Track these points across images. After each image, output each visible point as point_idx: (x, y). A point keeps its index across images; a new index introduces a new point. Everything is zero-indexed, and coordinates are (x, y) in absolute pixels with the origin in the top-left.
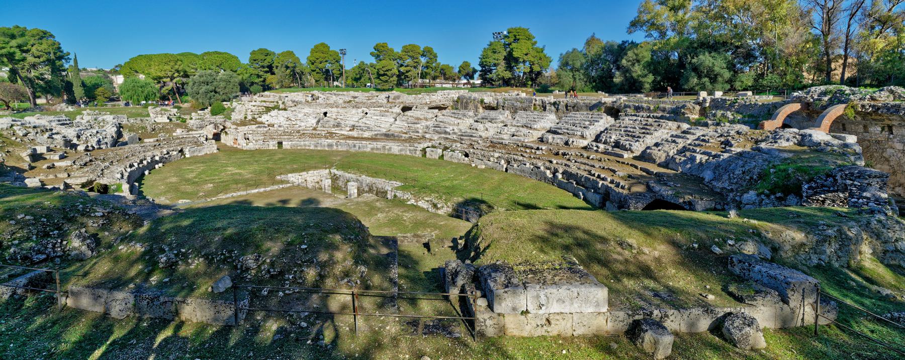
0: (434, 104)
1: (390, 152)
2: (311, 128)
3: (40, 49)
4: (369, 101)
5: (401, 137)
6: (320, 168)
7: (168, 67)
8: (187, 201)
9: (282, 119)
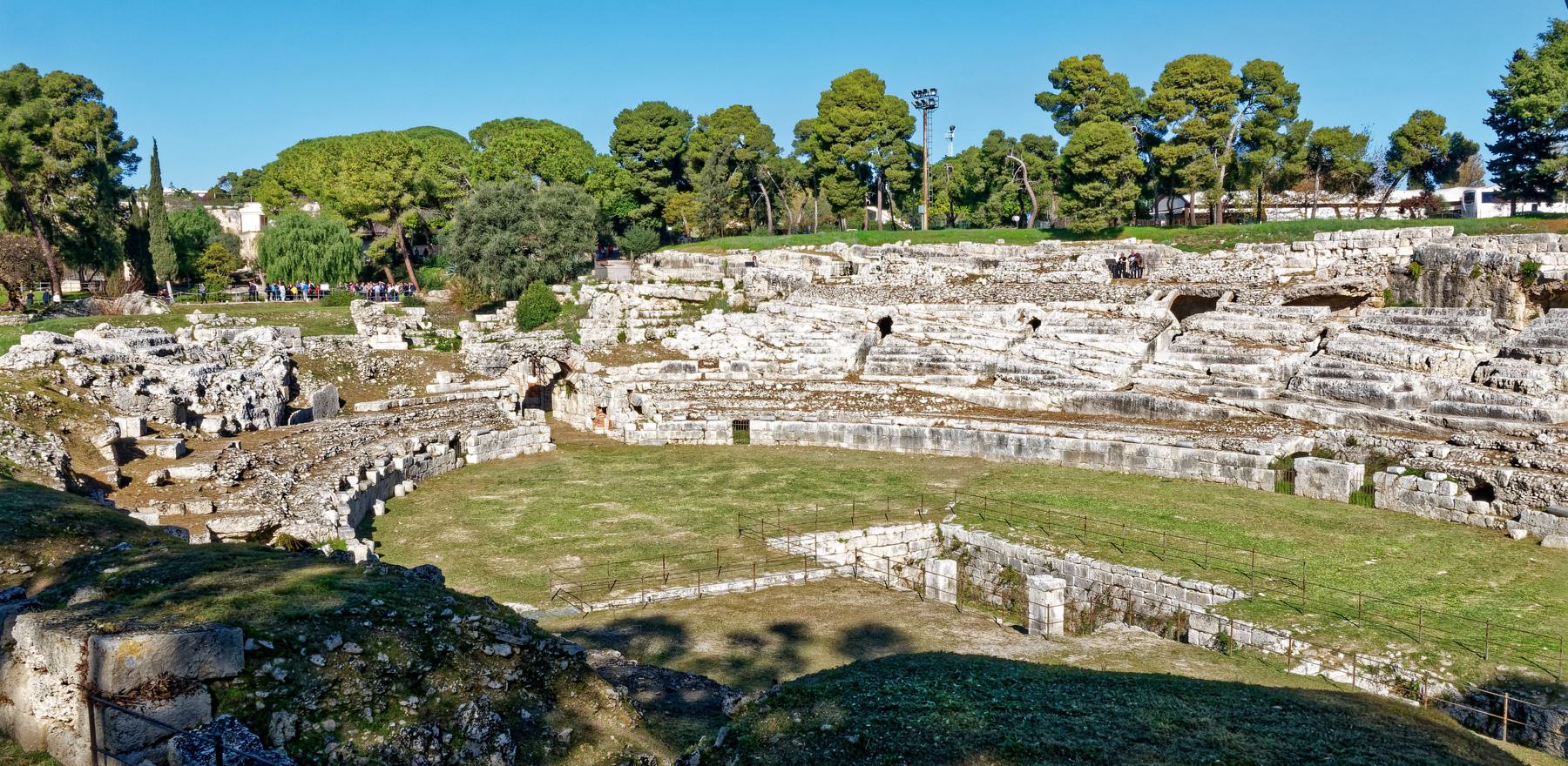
0: (1309, 286)
1: (1140, 470)
2: (841, 375)
3: (69, 130)
4: (1043, 278)
5: (1182, 411)
6: (902, 518)
7: (384, 176)
8: (116, 570)
9: (742, 342)
